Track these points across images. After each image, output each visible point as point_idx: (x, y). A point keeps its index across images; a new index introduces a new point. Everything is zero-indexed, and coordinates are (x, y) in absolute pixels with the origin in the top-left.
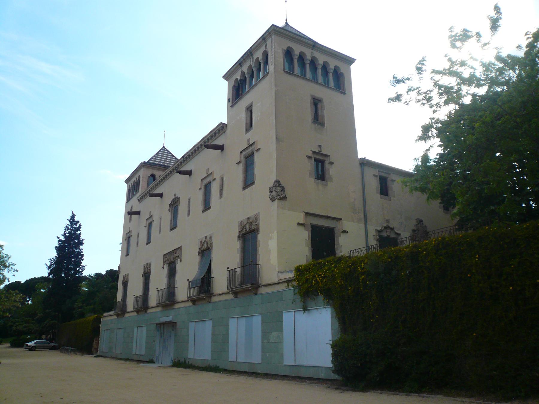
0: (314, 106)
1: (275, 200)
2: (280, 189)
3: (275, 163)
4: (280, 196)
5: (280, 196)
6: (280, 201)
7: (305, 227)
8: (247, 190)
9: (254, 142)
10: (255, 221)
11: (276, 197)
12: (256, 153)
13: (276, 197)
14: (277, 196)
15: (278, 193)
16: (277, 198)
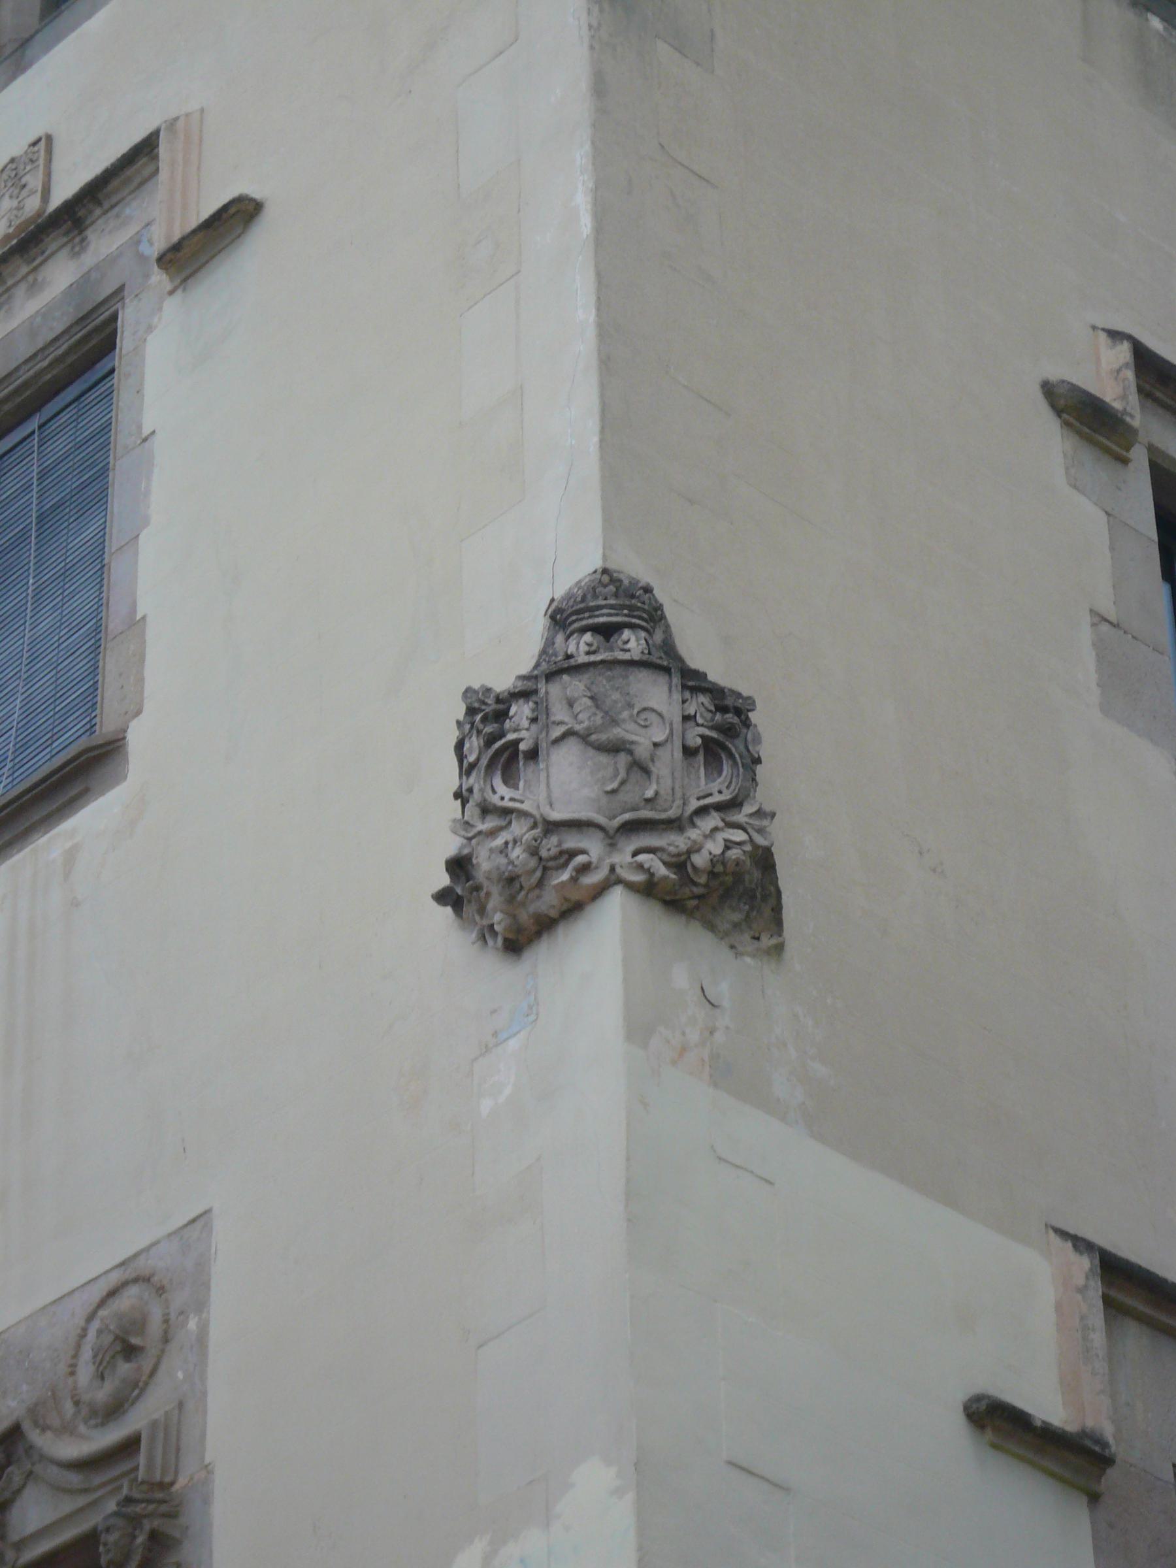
0: (590, 828)
1: (572, 909)
2: (674, 712)
3: (585, 314)
4: (676, 842)
5: (676, 842)
6: (668, 926)
7: (1094, 1498)
8: (152, 430)
9: (146, 149)
10: (102, 1394)
11: (612, 846)
12: (172, 306)
13: (612, 846)
14: (633, 827)
15: (641, 768)
16: (623, 857)
